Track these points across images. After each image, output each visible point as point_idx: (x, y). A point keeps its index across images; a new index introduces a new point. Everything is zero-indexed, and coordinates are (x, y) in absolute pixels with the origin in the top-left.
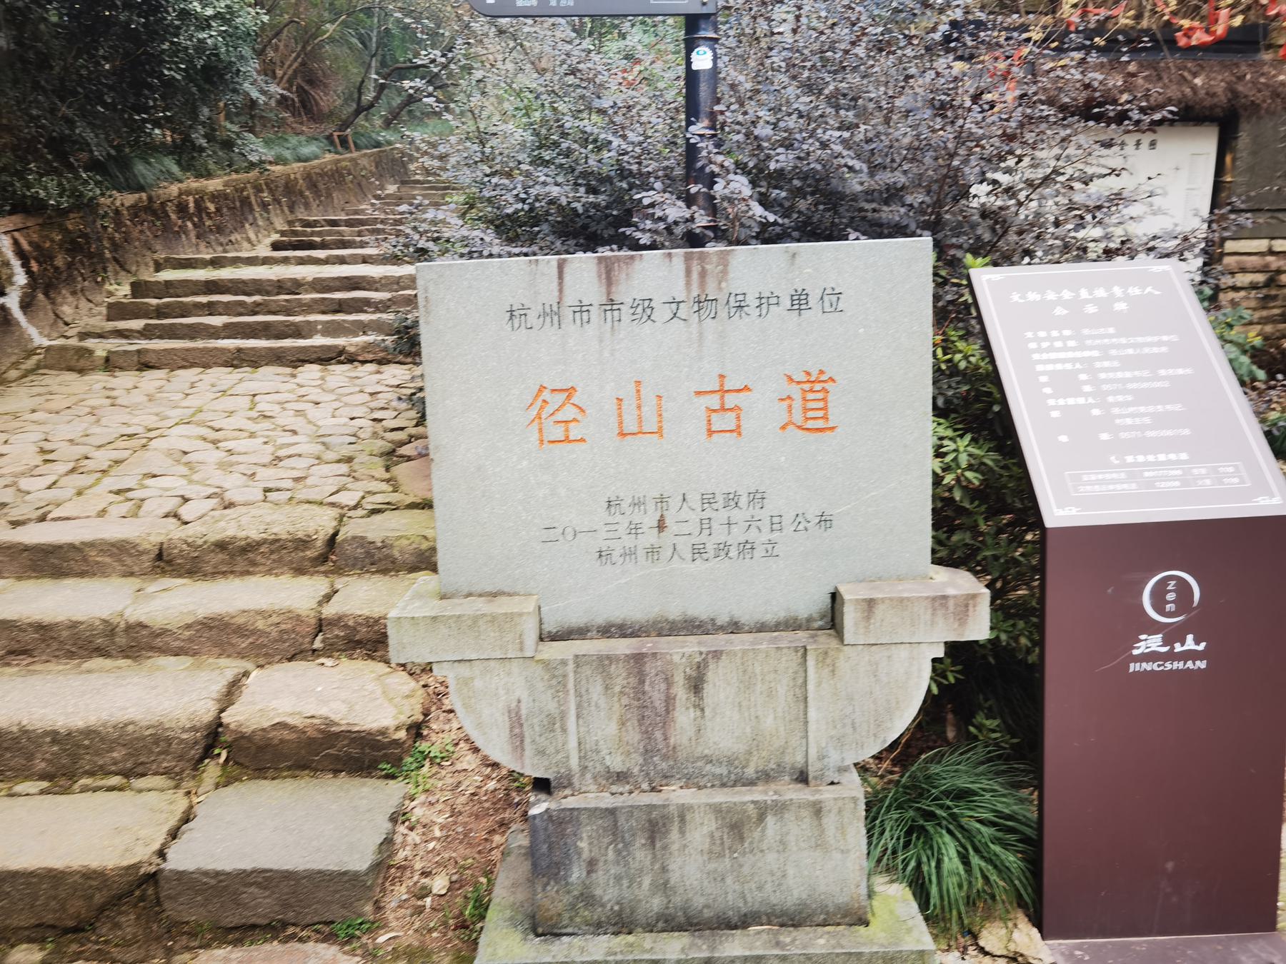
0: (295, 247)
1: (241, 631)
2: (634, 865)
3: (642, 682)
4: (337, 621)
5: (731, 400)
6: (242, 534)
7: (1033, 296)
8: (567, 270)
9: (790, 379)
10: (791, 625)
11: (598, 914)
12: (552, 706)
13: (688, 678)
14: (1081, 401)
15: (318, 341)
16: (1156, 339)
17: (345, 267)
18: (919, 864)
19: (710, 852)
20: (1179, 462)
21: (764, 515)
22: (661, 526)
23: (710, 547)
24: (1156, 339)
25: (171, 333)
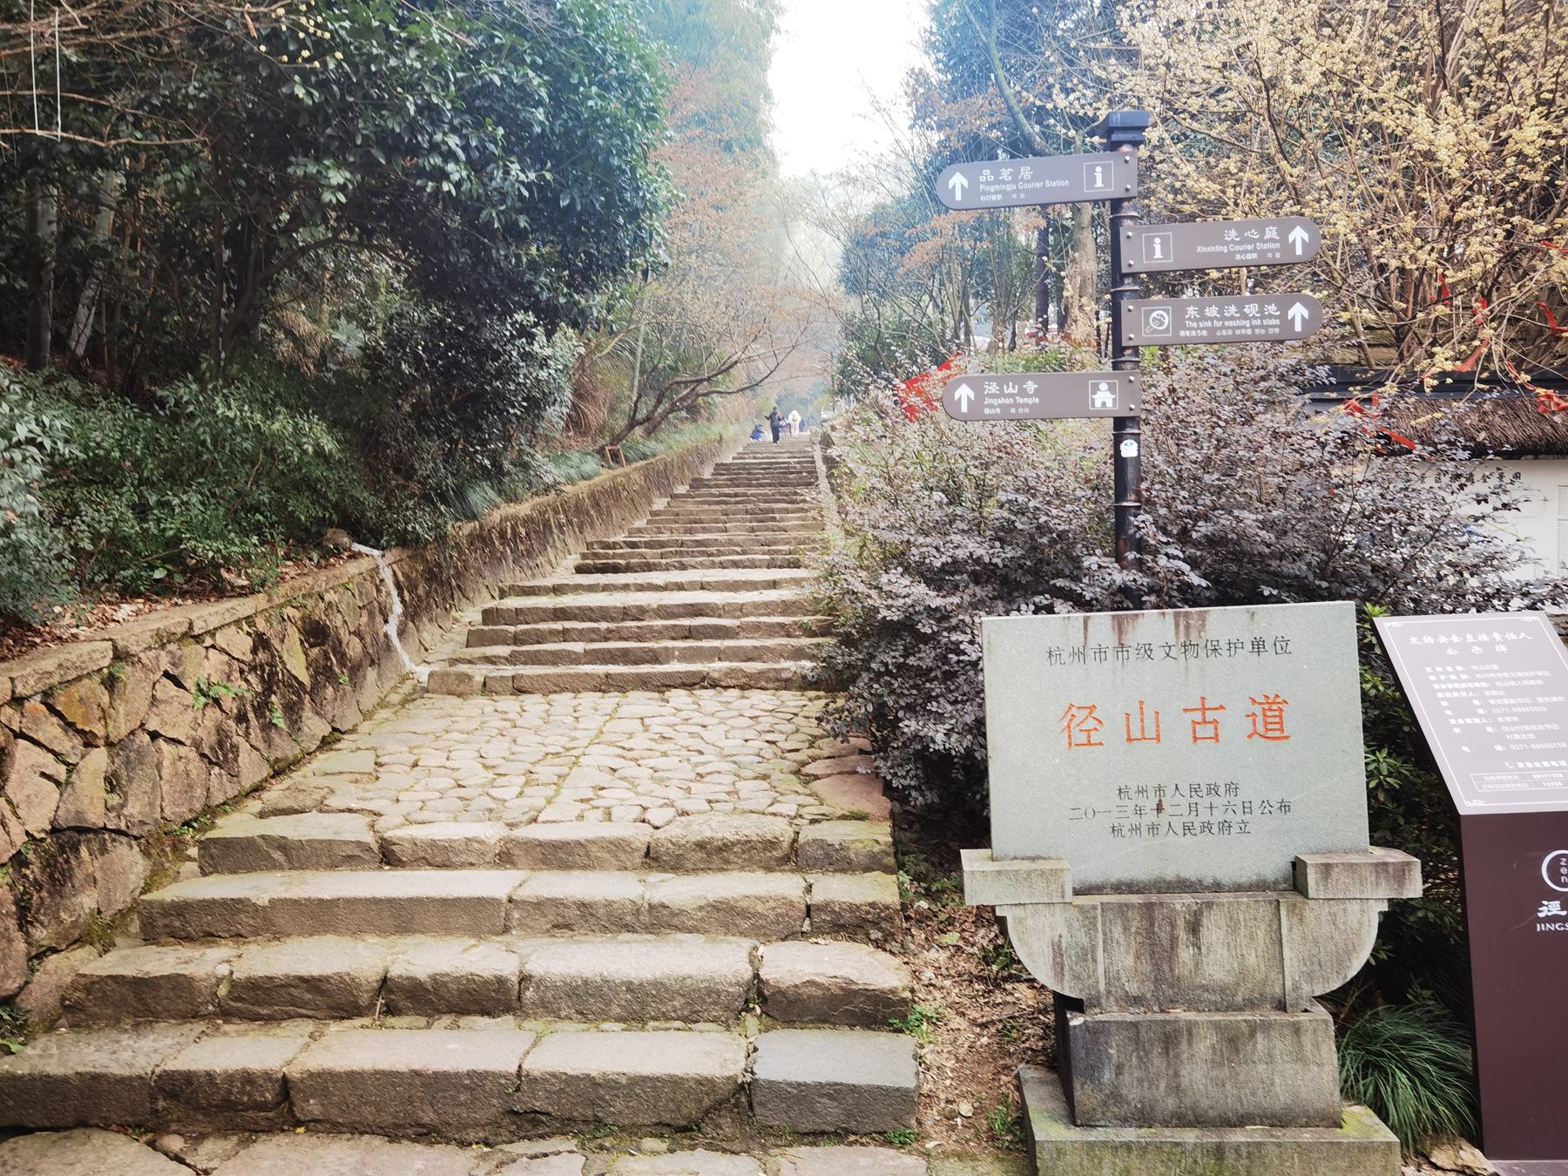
0: (604, 569)
1: (744, 913)
2: (1152, 1070)
3: (1152, 925)
4: (825, 907)
5: (1210, 716)
6: (719, 835)
7: (1428, 640)
8: (1090, 624)
9: (1254, 701)
10: (1260, 886)
11: (1124, 1110)
12: (1085, 941)
13: (1187, 922)
14: (1477, 721)
15: (675, 667)
16: (1532, 674)
17: (683, 594)
18: (1377, 1089)
19: (1213, 1061)
20: (1561, 768)
21: (1238, 801)
22: (1159, 808)
23: (1197, 825)
24: (1532, 674)
25: (535, 659)
